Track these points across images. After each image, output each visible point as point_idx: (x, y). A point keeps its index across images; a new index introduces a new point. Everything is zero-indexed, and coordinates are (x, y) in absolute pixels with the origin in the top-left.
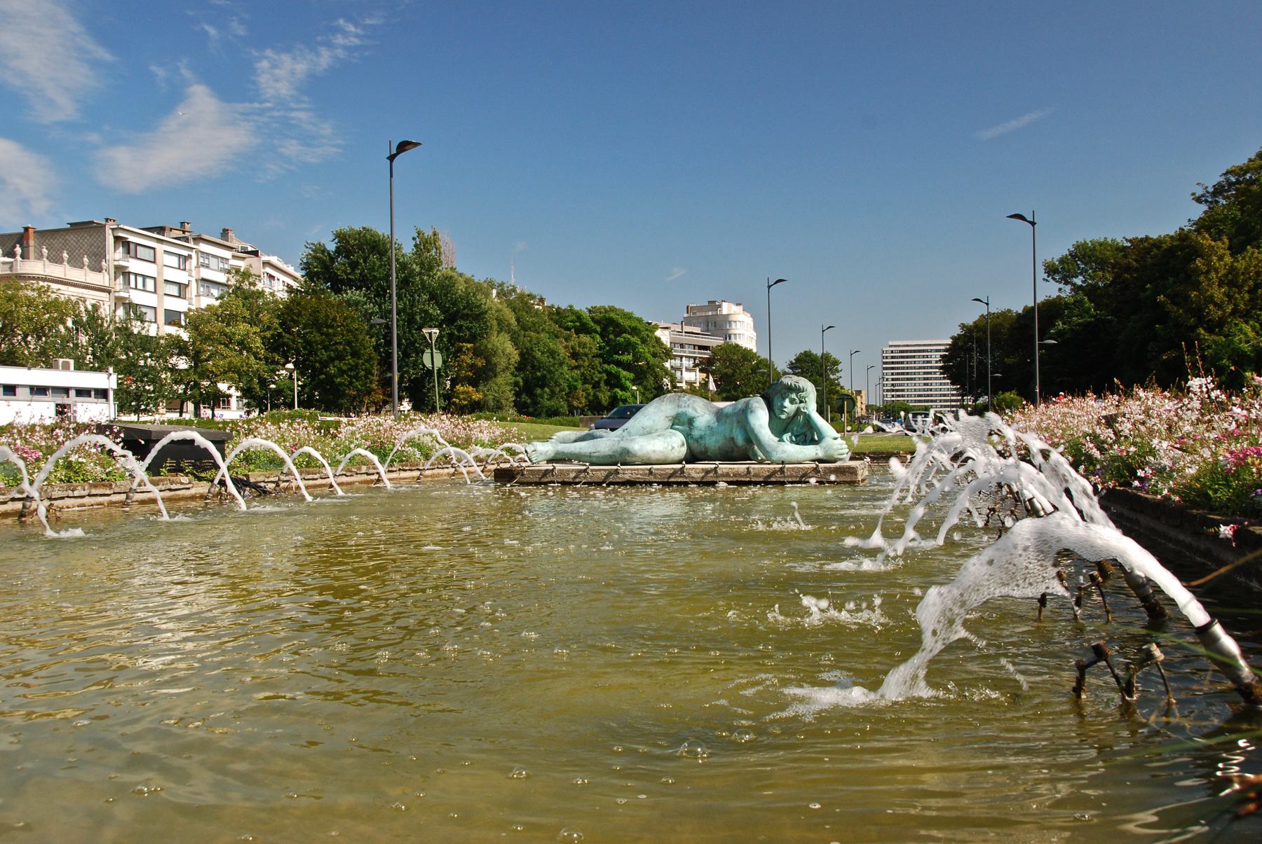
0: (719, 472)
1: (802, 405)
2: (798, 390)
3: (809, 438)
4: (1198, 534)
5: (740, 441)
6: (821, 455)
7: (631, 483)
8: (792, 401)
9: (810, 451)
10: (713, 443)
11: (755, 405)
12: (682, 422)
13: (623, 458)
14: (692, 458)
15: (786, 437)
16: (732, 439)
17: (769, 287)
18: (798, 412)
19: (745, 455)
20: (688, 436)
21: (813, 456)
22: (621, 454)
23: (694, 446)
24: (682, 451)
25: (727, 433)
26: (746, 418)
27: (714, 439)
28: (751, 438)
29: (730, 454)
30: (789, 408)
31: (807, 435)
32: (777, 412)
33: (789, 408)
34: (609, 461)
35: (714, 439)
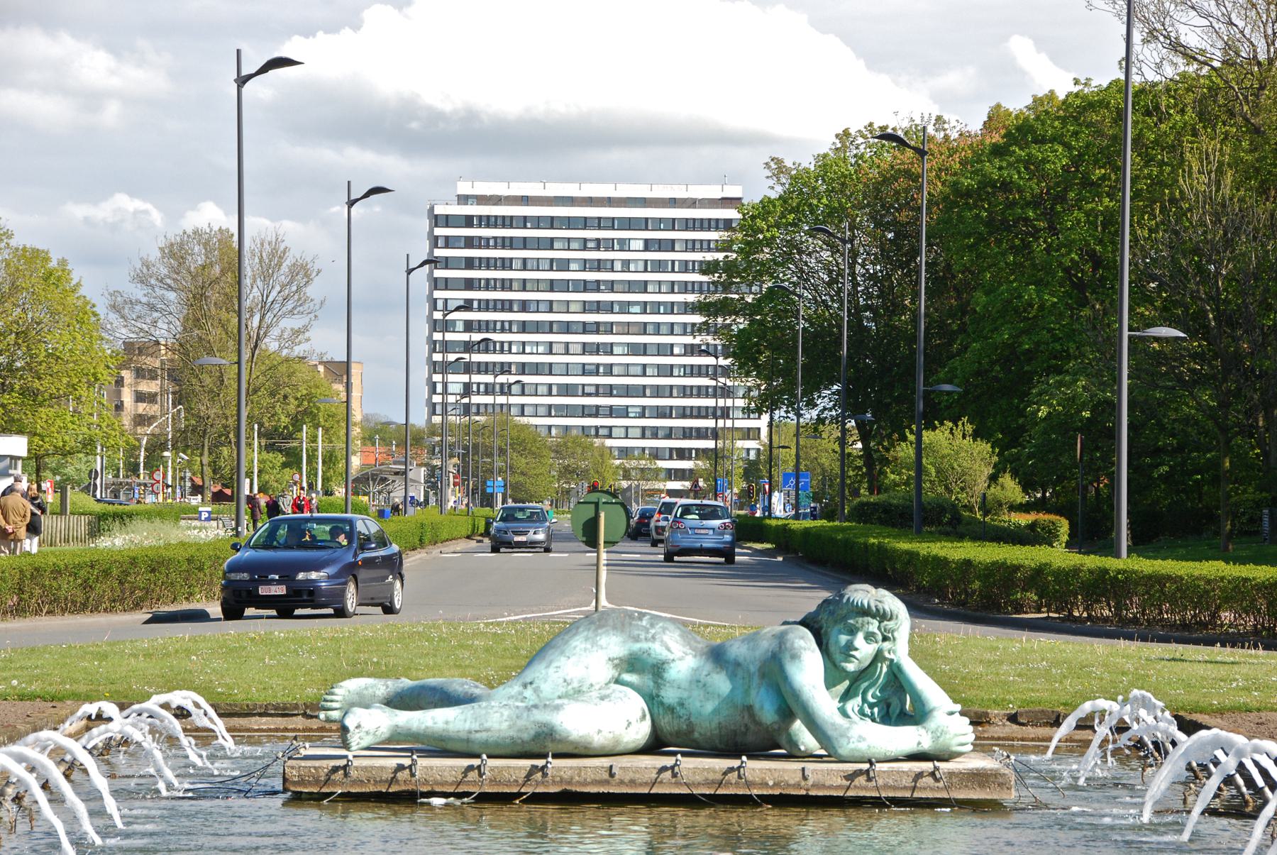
0: (354, 774)
1: (887, 645)
2: (882, 616)
3: (895, 710)
4: (1037, 424)
5: (768, 713)
6: (927, 745)
7: (569, 799)
8: (869, 637)
9: (905, 738)
11: (799, 643)
12: (642, 669)
13: (542, 745)
14: (655, 746)
15: (854, 704)
16: (749, 709)
17: (242, 81)
18: (878, 657)
19: (768, 743)
20: (652, 699)
21: (910, 747)
22: (537, 736)
23: (666, 723)
24: (640, 732)
26: (785, 678)
28: (791, 706)
29: (734, 743)
30: (864, 650)
31: (898, 706)
32: (838, 657)
33: (864, 650)
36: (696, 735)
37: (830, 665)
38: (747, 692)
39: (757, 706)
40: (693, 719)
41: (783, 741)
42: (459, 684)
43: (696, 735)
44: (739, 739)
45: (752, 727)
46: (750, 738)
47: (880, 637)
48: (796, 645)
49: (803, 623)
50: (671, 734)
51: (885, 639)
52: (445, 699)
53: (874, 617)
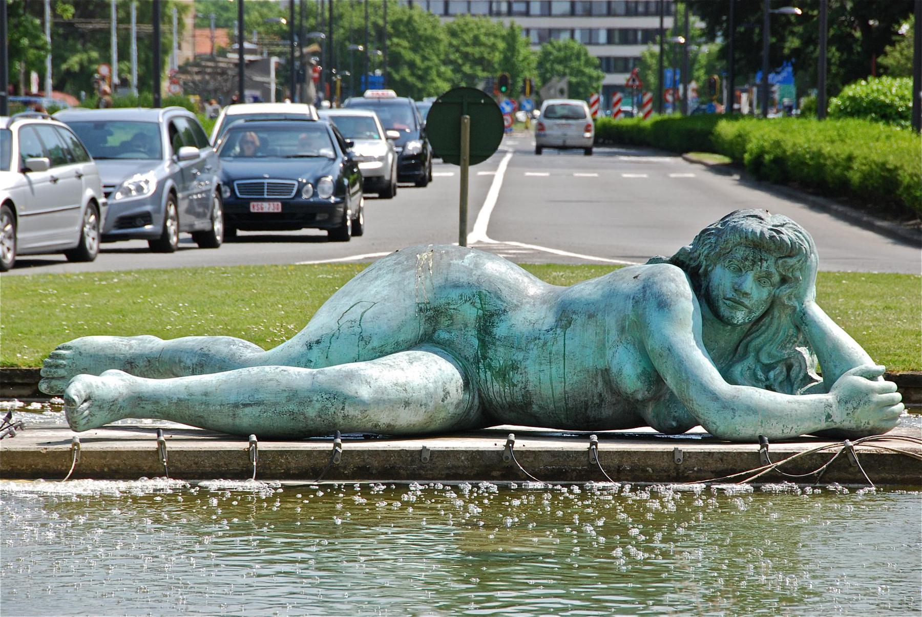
5: (630, 378)
6: (841, 419)
10: (545, 378)
16: (606, 372)
18: (773, 304)
23: (495, 389)
25: (591, 361)
27: (555, 370)
34: (267, 419)
35: (555, 370)
36: (535, 408)
37: (710, 315)
38: (602, 347)
39: (614, 370)
40: (530, 388)
41: (649, 412)
42: (222, 344)
43: (535, 408)
44: (592, 413)
45: (609, 398)
46: (607, 412)
47: (776, 278)
48: (664, 290)
49: (676, 261)
50: (502, 407)
51: (784, 280)
52: (205, 363)
53: (768, 251)
